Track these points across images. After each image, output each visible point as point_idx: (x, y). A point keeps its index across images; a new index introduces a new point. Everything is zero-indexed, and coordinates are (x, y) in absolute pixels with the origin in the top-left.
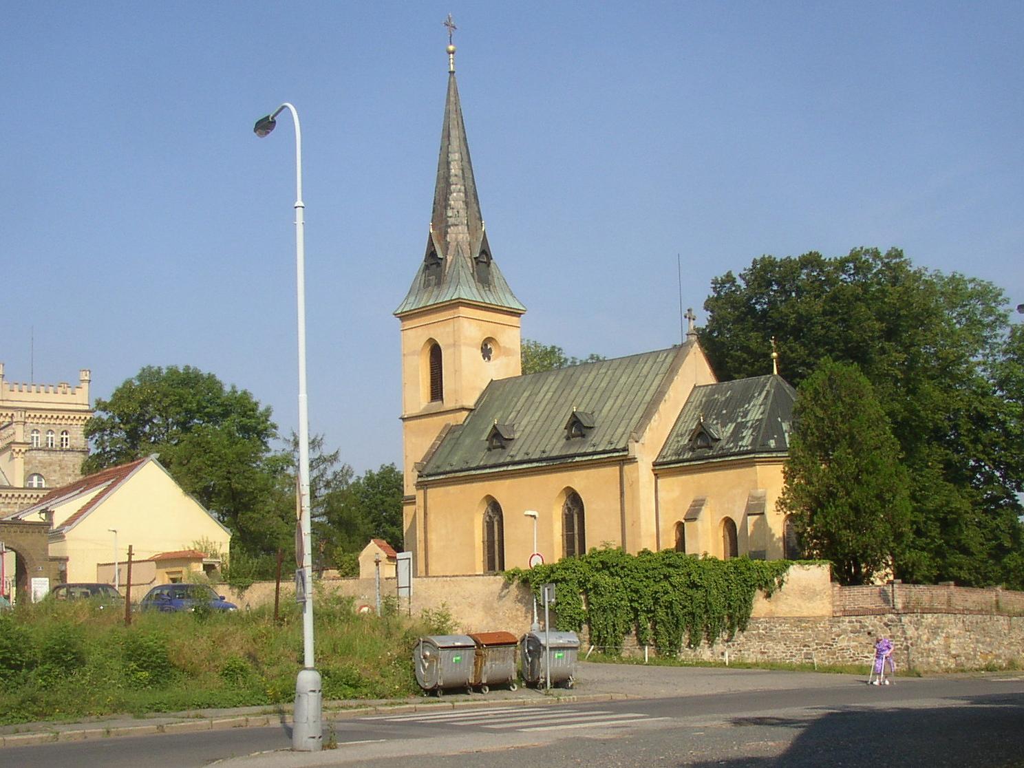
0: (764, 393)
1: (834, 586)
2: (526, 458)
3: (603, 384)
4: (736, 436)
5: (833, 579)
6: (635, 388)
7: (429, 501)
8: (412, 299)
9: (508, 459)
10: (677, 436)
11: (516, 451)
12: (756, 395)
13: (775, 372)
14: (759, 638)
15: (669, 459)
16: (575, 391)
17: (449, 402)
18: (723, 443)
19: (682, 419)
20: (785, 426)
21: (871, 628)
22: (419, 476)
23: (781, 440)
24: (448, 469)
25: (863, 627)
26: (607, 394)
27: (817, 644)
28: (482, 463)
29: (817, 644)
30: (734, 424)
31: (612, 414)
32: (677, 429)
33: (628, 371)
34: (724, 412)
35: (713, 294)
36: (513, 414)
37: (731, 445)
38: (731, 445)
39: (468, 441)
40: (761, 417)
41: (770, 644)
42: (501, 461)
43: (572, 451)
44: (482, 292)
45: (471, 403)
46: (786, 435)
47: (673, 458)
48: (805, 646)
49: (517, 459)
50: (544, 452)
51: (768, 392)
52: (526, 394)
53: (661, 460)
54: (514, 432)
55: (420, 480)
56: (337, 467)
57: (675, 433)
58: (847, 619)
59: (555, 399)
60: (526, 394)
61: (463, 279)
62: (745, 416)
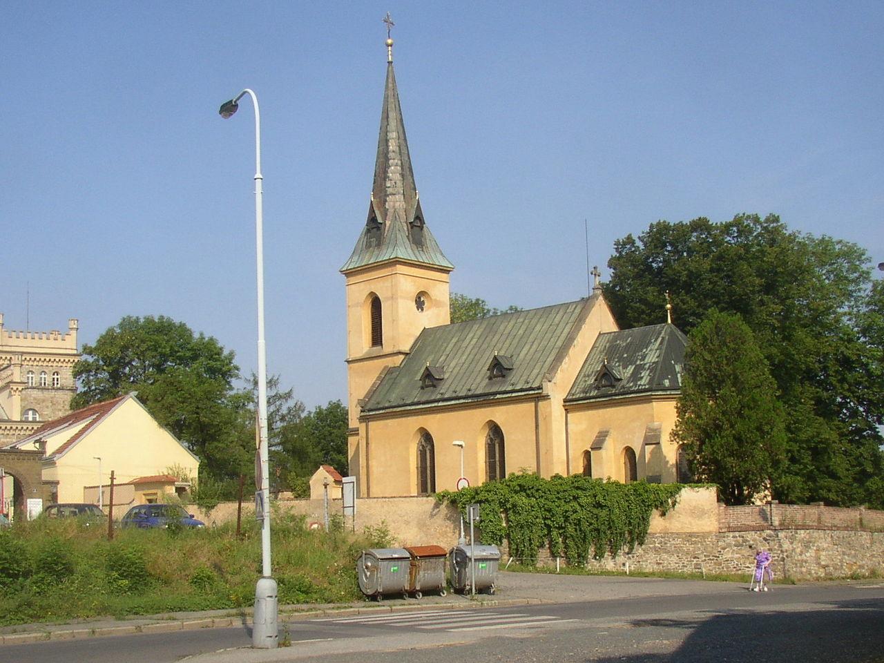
0: (660, 339)
2: (454, 395)
3: (521, 332)
4: (635, 376)
5: (719, 500)
6: (548, 335)
9: (439, 397)
10: (585, 376)
11: (445, 390)
12: (653, 341)
13: (669, 321)
14: (656, 551)
16: (497, 337)
17: (387, 347)
18: (624, 382)
19: (588, 362)
20: (678, 368)
21: (752, 542)
22: (362, 411)
23: (674, 380)
24: (386, 405)
25: (745, 541)
31: (529, 357)
35: (615, 254)
36: (443, 358)
38: (631, 384)
40: (657, 360)
43: (494, 390)
45: (406, 348)
46: (679, 375)
47: (582, 395)
49: (446, 396)
51: (663, 338)
52: (454, 340)
53: (571, 397)
54: (444, 373)
55: (362, 414)
56: (291, 403)
57: (583, 374)
58: (731, 534)
60: (454, 340)
62: (643, 358)
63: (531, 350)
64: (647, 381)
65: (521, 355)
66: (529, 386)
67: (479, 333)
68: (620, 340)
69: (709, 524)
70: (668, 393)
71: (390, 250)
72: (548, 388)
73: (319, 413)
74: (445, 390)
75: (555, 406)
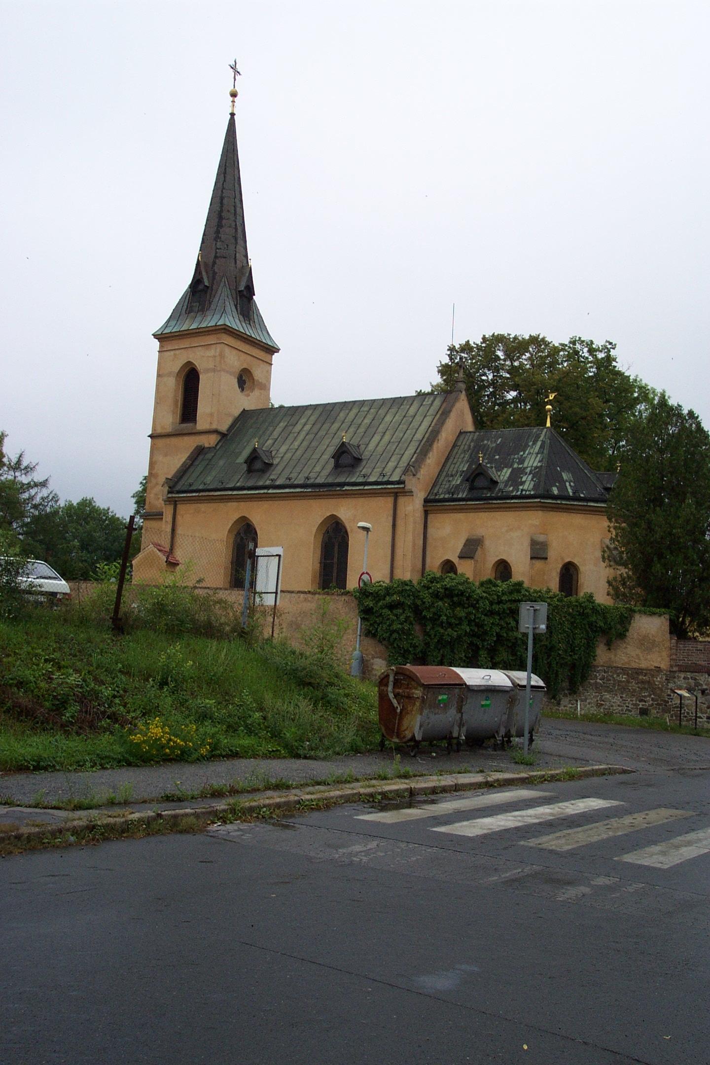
0: (539, 443)
1: (671, 639)
2: (288, 482)
3: (367, 421)
4: (515, 478)
5: (671, 633)
6: (403, 427)
7: (179, 518)
8: (173, 323)
9: (268, 483)
10: (447, 475)
11: (278, 475)
12: (531, 444)
13: (548, 424)
14: (596, 688)
15: (442, 497)
16: (336, 425)
17: (202, 423)
18: (501, 486)
19: (451, 460)
20: (565, 476)
21: (705, 687)
22: (169, 492)
23: (563, 487)
24: (201, 487)
25: (697, 684)
26: (372, 430)
27: (653, 699)
28: (238, 484)
29: (653, 699)
30: (510, 470)
31: (380, 449)
32: (446, 469)
33: (393, 410)
34: (497, 457)
35: (446, 360)
36: (270, 442)
37: (511, 489)
38: (511, 489)
39: (221, 463)
40: (539, 464)
41: (607, 696)
42: (261, 483)
43: (341, 479)
44: (244, 324)
45: (224, 428)
46: (567, 484)
47: (447, 496)
48: (641, 701)
49: (278, 483)
50: (308, 478)
51: (543, 442)
52: (282, 424)
53: (432, 497)
54: (272, 458)
55: (170, 495)
56: (44, 492)
57: (444, 473)
58: (682, 675)
59: (315, 430)
60: (282, 424)
61: (228, 309)
62: (522, 461)
63: (383, 440)
64: (531, 486)
65: (370, 445)
66: (385, 479)
67: (313, 418)
68: (488, 440)
69: (659, 659)
70: (559, 502)
71: (216, 317)
72: (411, 483)
73: (70, 507)
74: (278, 475)
75: (412, 507)
